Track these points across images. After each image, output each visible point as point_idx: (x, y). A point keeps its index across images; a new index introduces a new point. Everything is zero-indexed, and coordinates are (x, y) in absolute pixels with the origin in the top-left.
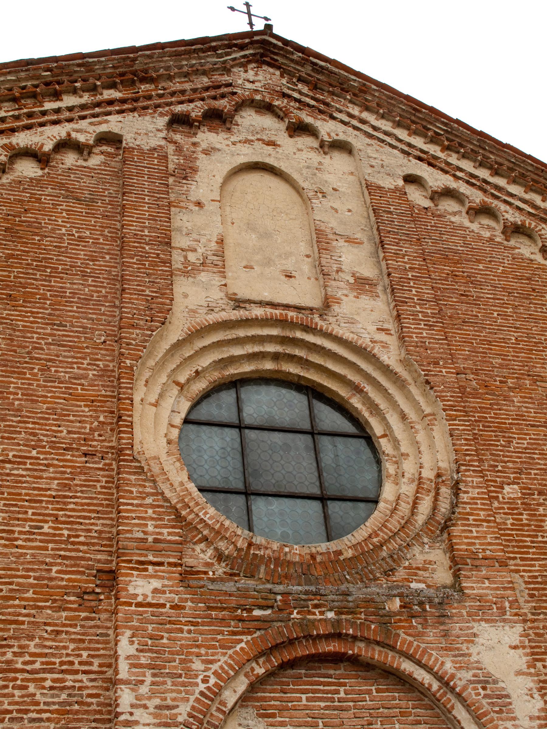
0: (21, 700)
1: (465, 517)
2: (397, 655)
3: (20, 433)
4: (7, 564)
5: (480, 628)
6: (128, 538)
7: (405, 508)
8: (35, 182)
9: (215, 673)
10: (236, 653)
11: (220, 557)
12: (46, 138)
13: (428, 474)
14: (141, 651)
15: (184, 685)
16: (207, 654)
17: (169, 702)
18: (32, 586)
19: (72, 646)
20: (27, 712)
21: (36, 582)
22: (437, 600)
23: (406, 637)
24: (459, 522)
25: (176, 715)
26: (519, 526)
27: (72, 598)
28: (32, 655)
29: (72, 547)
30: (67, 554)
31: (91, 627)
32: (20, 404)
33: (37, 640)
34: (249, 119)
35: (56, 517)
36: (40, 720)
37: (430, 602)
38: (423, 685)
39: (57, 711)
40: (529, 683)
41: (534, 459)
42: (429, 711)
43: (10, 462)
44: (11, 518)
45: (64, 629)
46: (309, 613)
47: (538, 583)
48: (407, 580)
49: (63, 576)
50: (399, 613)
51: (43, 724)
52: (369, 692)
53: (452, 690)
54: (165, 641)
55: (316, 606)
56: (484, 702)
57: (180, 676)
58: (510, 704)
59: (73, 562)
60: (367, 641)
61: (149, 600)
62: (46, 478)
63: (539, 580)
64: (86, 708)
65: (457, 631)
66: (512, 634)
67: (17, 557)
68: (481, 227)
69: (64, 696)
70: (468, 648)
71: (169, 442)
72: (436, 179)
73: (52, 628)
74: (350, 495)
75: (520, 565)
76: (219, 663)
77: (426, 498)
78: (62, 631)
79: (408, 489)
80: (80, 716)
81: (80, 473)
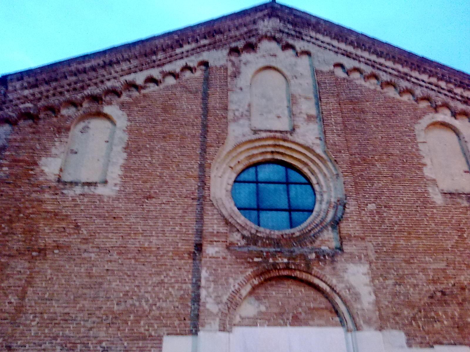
1: (347, 219)
7: (322, 214)
8: (174, 86)
11: (244, 237)
12: (176, 66)
13: (333, 200)
26: (374, 222)
34: (266, 46)
35: (181, 224)
37: (328, 255)
40: (370, 289)
41: (383, 192)
52: (301, 291)
53: (335, 291)
60: (300, 271)
66: (364, 268)
68: (372, 84)
71: (227, 191)
72: (349, 63)
74: (301, 208)
79: (324, 206)
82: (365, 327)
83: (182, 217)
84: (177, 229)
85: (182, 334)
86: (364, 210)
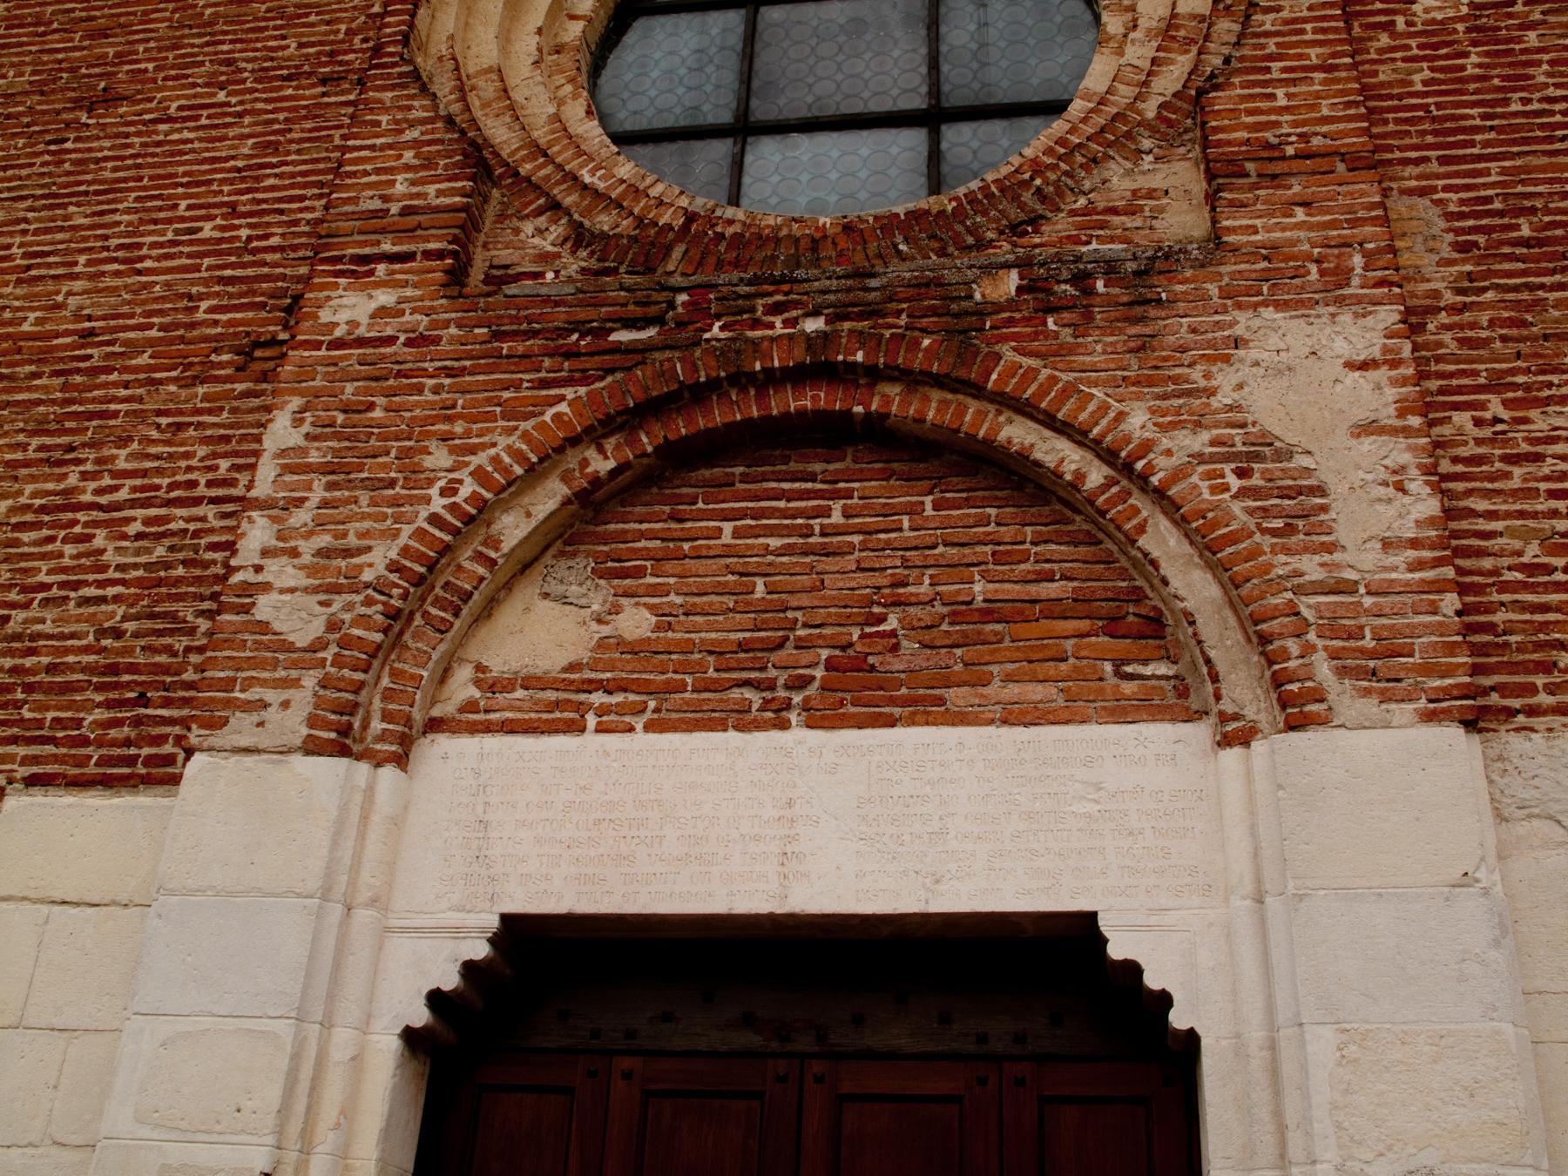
0: (75, 562)
2: (992, 408)
3: (202, 63)
4: (115, 307)
5: (1257, 323)
6: (346, 214)
9: (479, 475)
10: (542, 426)
14: (315, 438)
15: (396, 502)
16: (467, 434)
17: (352, 541)
18: (151, 343)
19: (202, 451)
20: (76, 586)
21: (161, 334)
22: (1131, 266)
23: (1019, 358)
24: (1236, 80)
25: (360, 568)
27: (225, 357)
28: (116, 474)
29: (251, 258)
30: (239, 273)
31: (251, 411)
32: (216, 13)
33: (135, 445)
36: (103, 600)
38: (1060, 477)
39: (138, 582)
42: (1082, 549)
43: (170, 120)
44: (142, 222)
45: (195, 419)
46: (756, 324)
47: (1490, 214)
48: (1076, 240)
49: (217, 317)
50: (1011, 304)
51: (103, 608)
52: (914, 510)
53: (1142, 480)
54: (378, 413)
55: (776, 309)
56: (1236, 508)
57: (392, 483)
58: (1324, 509)
59: (244, 288)
60: (913, 380)
61: (362, 331)
62: (234, 138)
63: (1497, 205)
64: (198, 572)
65: (1185, 336)
67: (135, 292)
69: (160, 551)
70: (1207, 376)
73: (170, 420)
75: (1438, 177)
76: (493, 451)
77: (1181, 58)
78: (191, 424)
80: (183, 589)
81: (305, 118)
82: (1343, 697)
83: (249, 176)
84: (208, 231)
85: (107, 783)
86: (1389, 27)
